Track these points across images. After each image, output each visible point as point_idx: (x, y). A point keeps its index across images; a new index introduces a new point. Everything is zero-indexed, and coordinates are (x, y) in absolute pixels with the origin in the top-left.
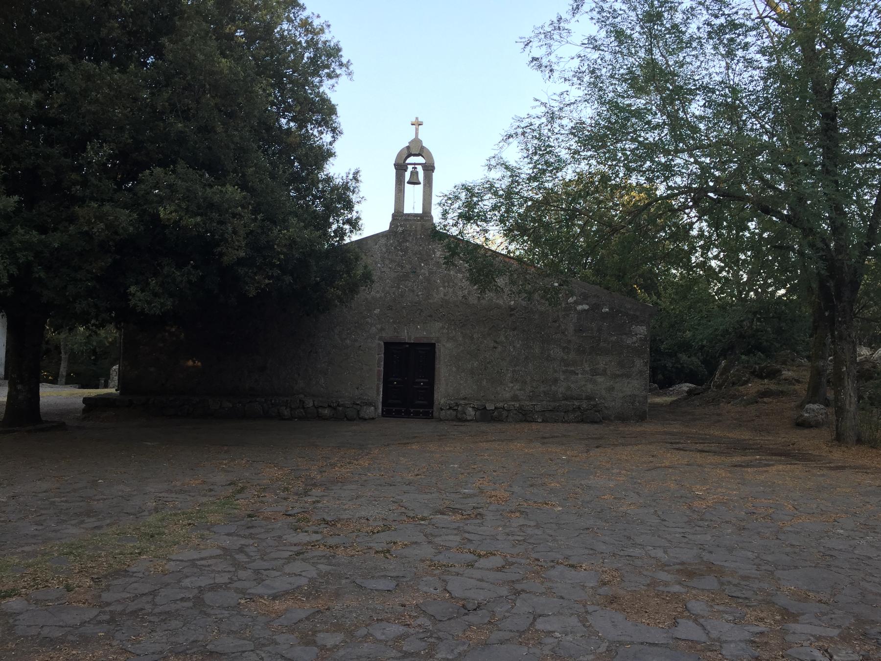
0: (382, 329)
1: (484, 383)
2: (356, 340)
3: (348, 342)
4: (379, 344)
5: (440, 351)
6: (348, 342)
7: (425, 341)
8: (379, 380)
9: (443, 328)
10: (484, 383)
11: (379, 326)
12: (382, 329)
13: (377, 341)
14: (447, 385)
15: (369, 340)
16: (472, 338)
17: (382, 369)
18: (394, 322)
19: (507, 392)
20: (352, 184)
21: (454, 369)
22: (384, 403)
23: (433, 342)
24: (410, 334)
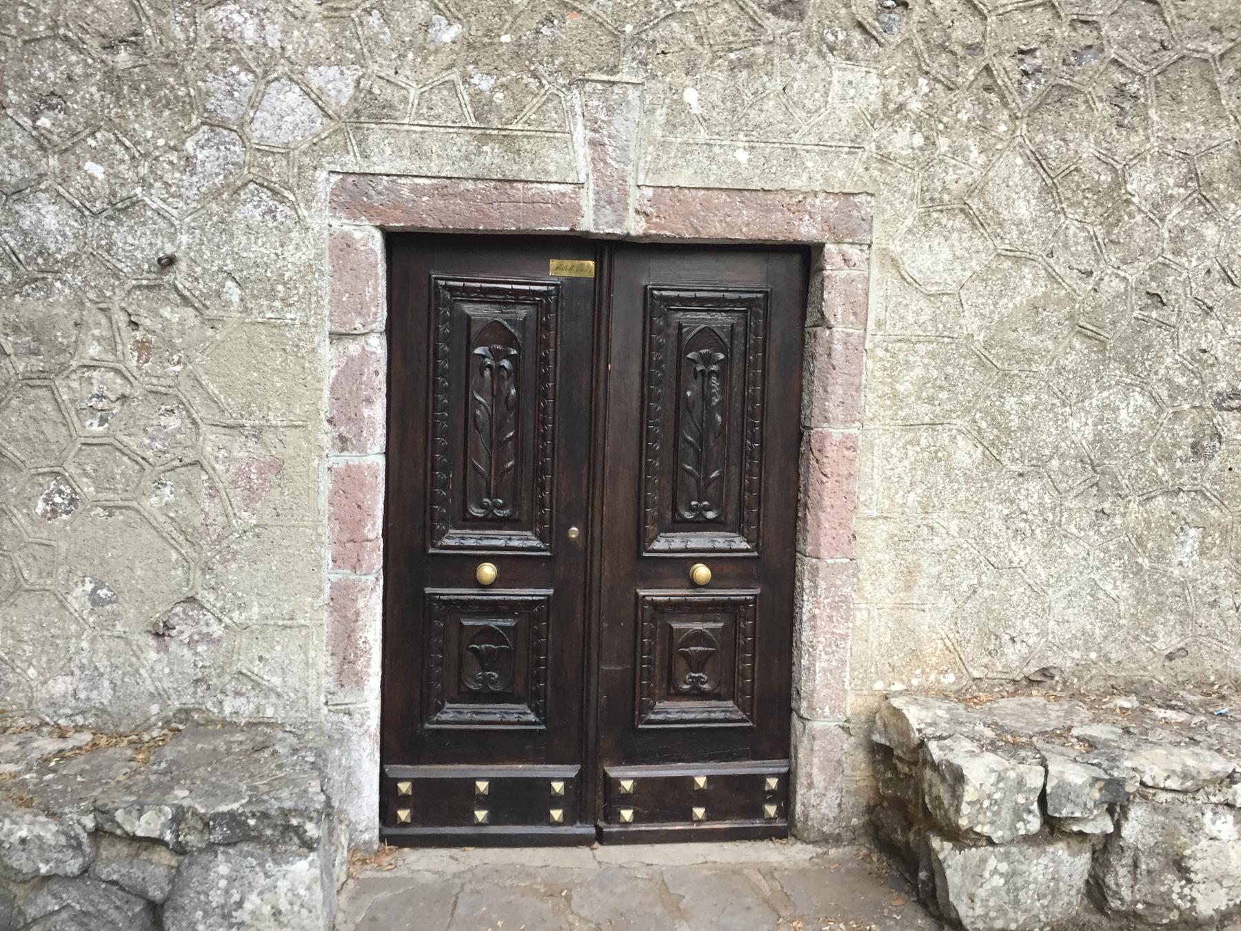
0: (369, 111)
1: (1185, 552)
2: (123, 208)
3: (48, 218)
4: (344, 246)
5: (859, 311)
6: (48, 218)
7: (745, 224)
8: (347, 557)
9: (894, 112)
10: (1185, 552)
11: (338, 84)
12: (369, 111)
13: (323, 221)
14: (909, 576)
15: (249, 212)
16: (1113, 200)
17: (374, 458)
18: (474, 49)
19: (520, 186)
20: (847, 835)
21: (966, 454)
22: (402, 736)
23: (806, 231)
24: (624, 158)
